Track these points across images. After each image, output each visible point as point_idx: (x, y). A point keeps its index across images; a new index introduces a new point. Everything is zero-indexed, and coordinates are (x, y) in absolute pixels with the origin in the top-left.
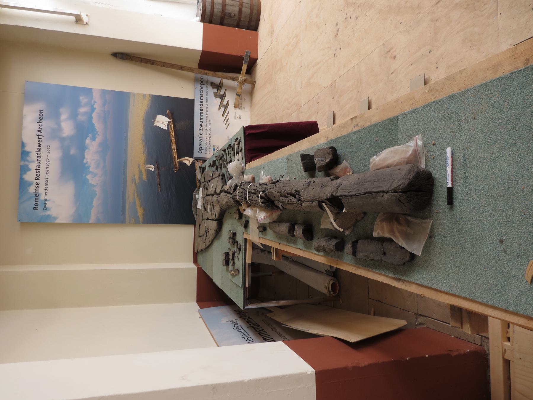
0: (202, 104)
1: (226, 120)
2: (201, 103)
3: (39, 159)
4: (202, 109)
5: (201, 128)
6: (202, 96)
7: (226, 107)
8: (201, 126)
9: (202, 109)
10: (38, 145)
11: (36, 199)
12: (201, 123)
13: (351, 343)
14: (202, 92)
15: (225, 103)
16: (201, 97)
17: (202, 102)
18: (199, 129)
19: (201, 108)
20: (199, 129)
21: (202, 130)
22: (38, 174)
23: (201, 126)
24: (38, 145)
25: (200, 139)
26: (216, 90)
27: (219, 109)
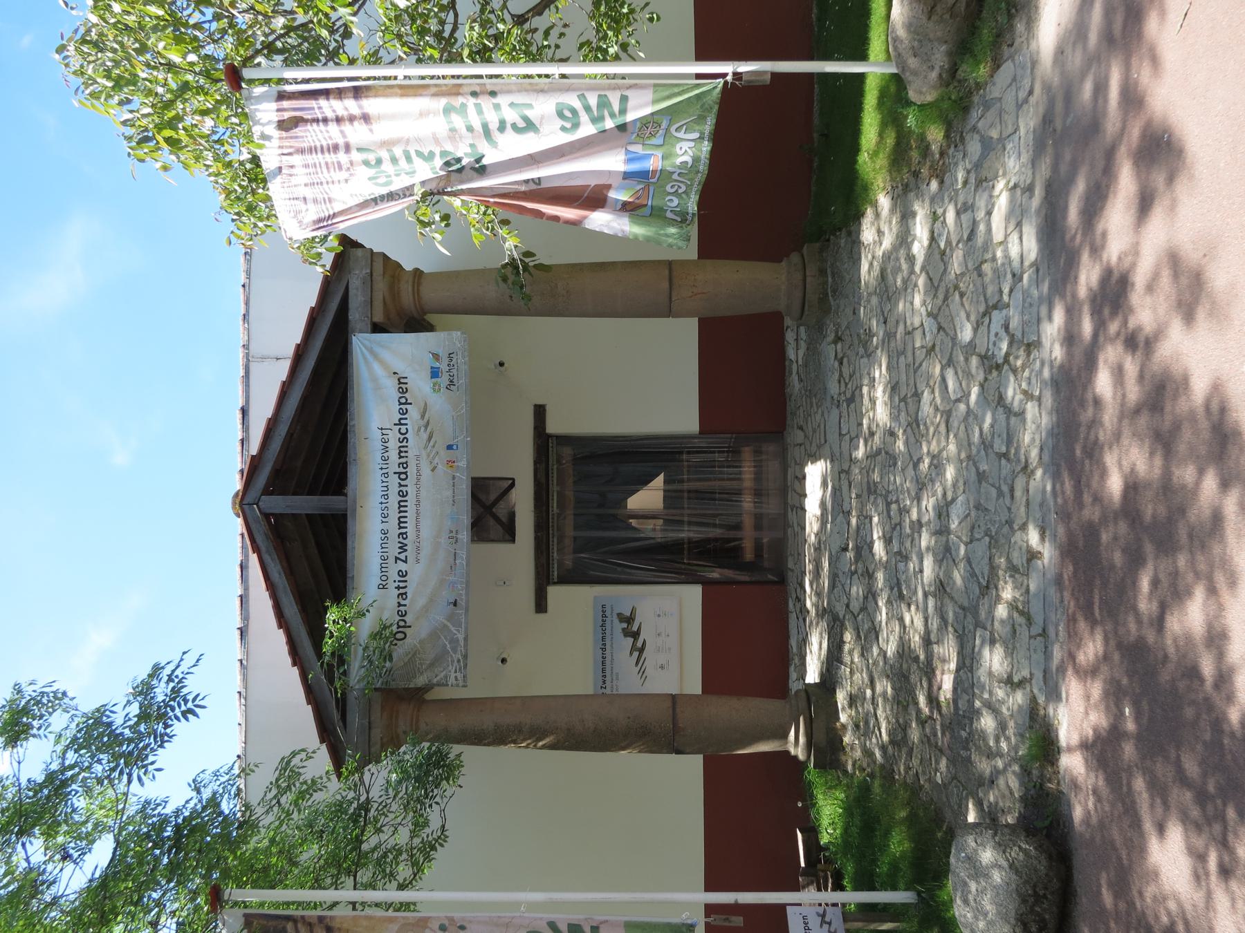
0: (405, 473)
1: (642, 672)
2: (402, 470)
3: (385, 480)
4: (404, 489)
5: (402, 556)
6: (404, 444)
7: (641, 650)
8: (403, 548)
9: (404, 489)
10: (400, 548)
11: (402, 504)
12: (401, 540)
13: (982, 154)
14: (403, 431)
15: (639, 644)
16: (402, 520)
17: (605, 645)
18: (397, 558)
19: (400, 485)
20: (397, 558)
21: (405, 561)
22: (385, 512)
23: (604, 682)
24: (400, 548)
25: (397, 592)
26: (625, 625)
27: (631, 654)
